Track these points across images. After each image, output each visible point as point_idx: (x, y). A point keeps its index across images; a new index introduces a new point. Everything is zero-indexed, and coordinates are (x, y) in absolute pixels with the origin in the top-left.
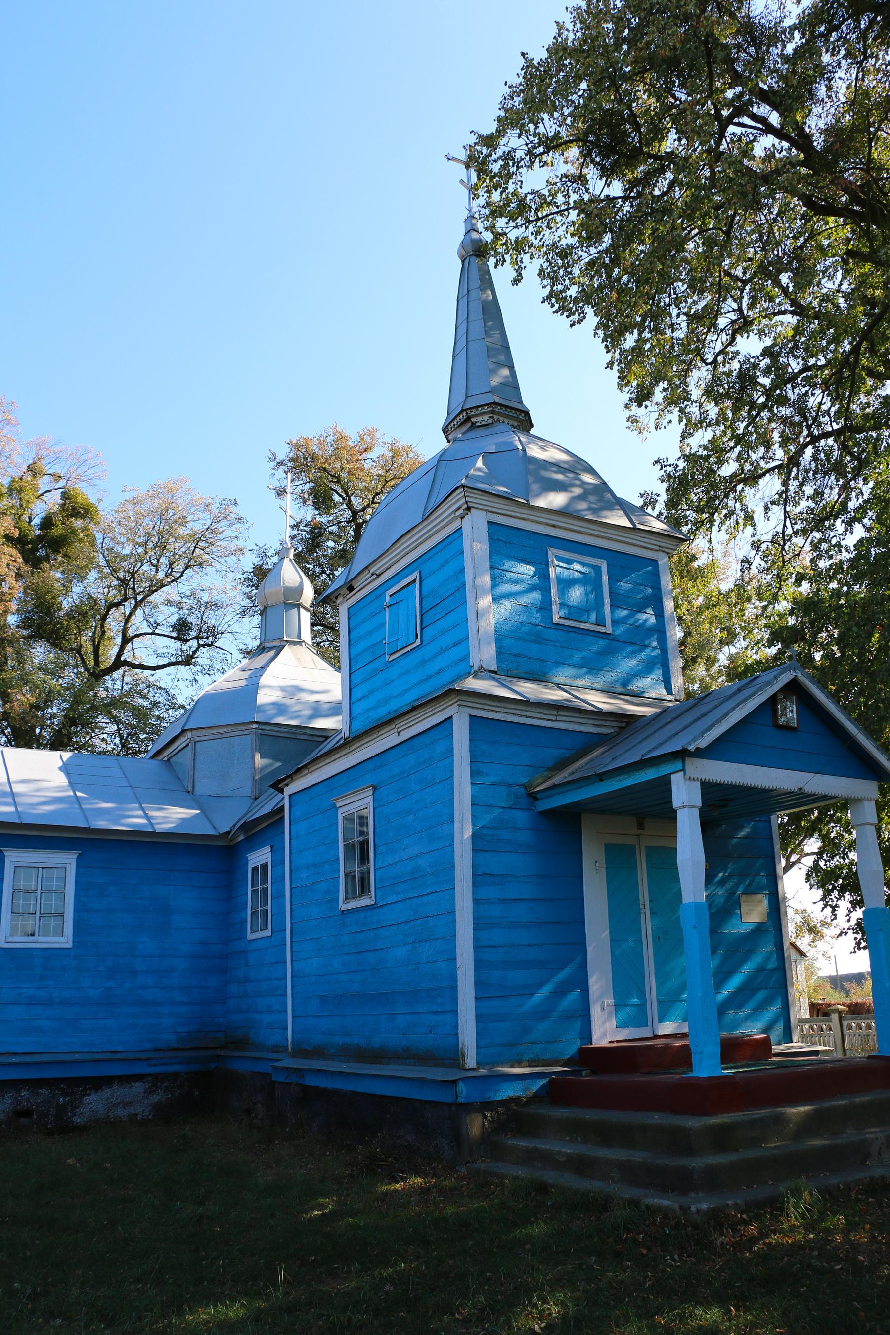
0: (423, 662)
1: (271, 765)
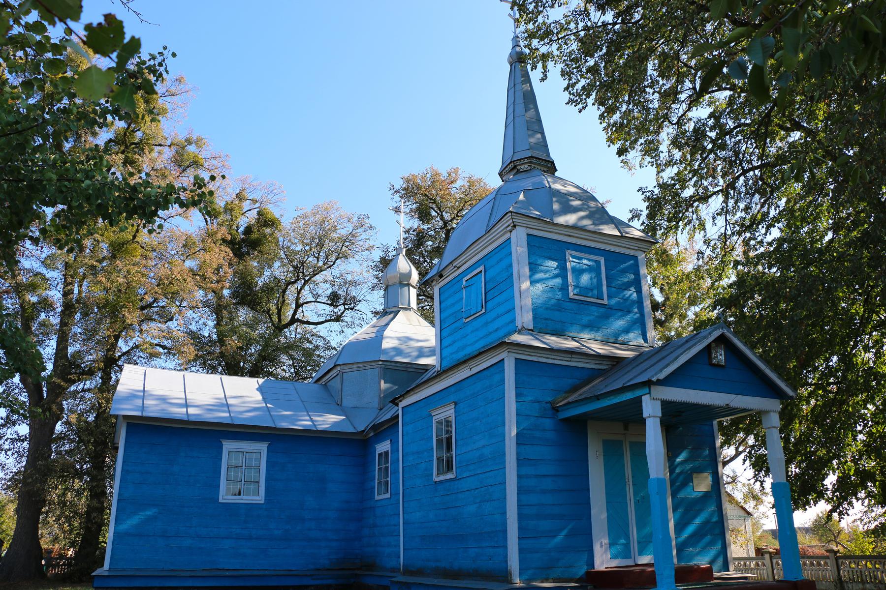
0: (487, 324)
1: (391, 388)
